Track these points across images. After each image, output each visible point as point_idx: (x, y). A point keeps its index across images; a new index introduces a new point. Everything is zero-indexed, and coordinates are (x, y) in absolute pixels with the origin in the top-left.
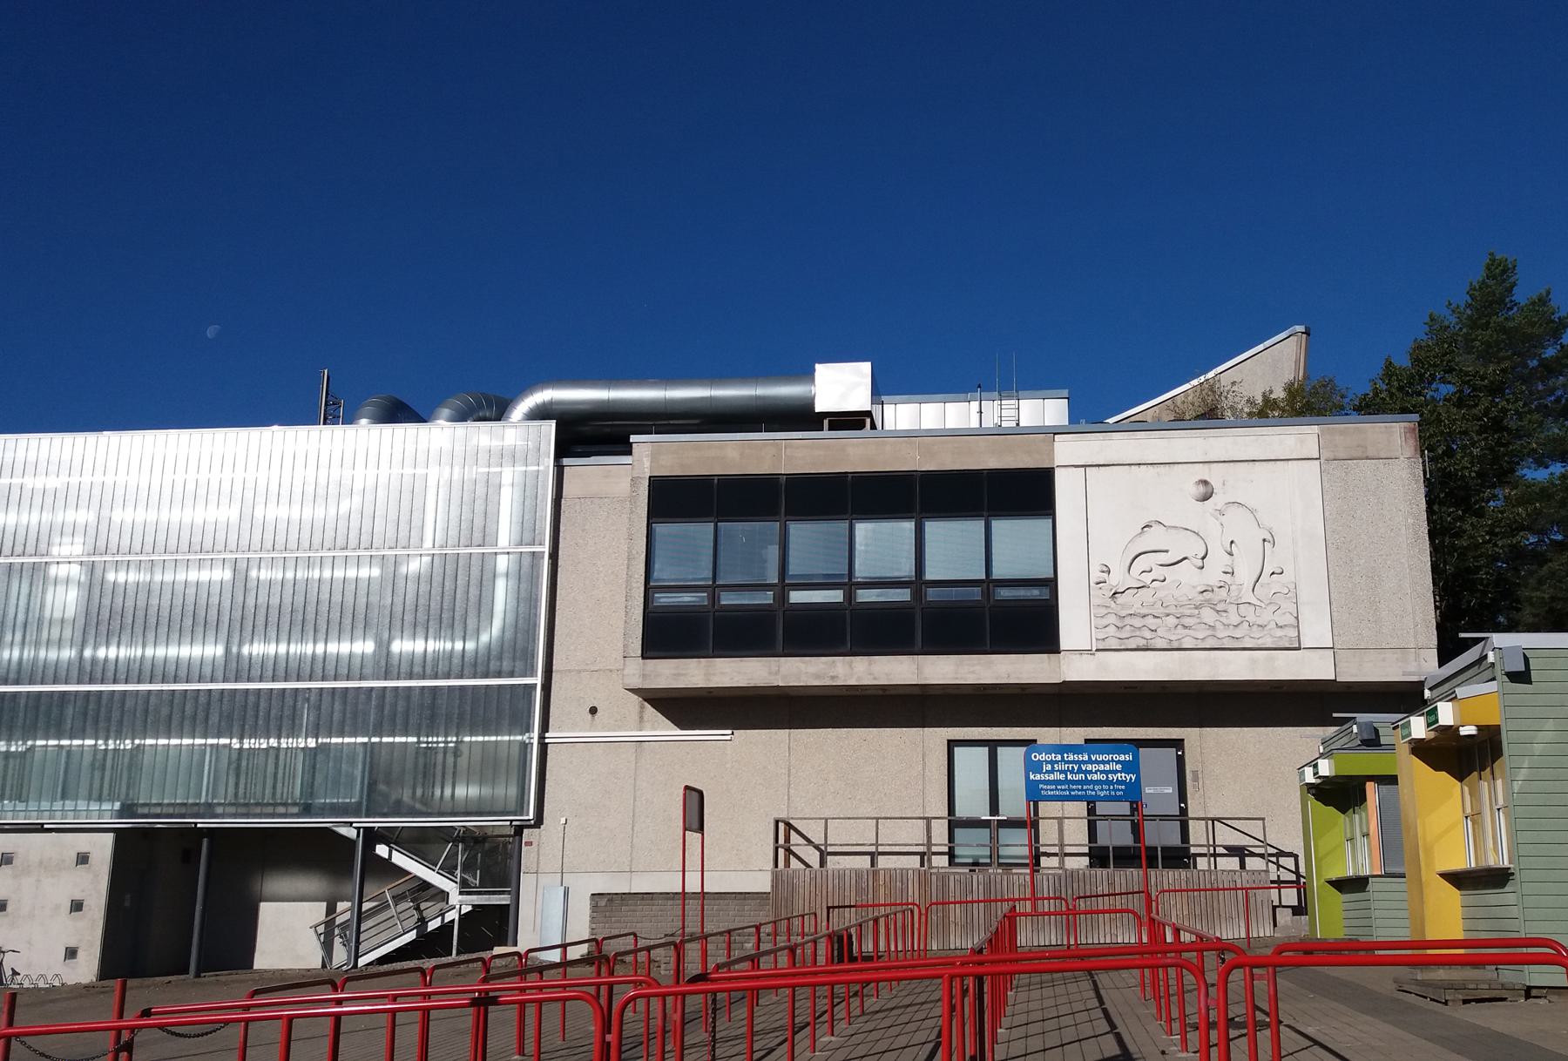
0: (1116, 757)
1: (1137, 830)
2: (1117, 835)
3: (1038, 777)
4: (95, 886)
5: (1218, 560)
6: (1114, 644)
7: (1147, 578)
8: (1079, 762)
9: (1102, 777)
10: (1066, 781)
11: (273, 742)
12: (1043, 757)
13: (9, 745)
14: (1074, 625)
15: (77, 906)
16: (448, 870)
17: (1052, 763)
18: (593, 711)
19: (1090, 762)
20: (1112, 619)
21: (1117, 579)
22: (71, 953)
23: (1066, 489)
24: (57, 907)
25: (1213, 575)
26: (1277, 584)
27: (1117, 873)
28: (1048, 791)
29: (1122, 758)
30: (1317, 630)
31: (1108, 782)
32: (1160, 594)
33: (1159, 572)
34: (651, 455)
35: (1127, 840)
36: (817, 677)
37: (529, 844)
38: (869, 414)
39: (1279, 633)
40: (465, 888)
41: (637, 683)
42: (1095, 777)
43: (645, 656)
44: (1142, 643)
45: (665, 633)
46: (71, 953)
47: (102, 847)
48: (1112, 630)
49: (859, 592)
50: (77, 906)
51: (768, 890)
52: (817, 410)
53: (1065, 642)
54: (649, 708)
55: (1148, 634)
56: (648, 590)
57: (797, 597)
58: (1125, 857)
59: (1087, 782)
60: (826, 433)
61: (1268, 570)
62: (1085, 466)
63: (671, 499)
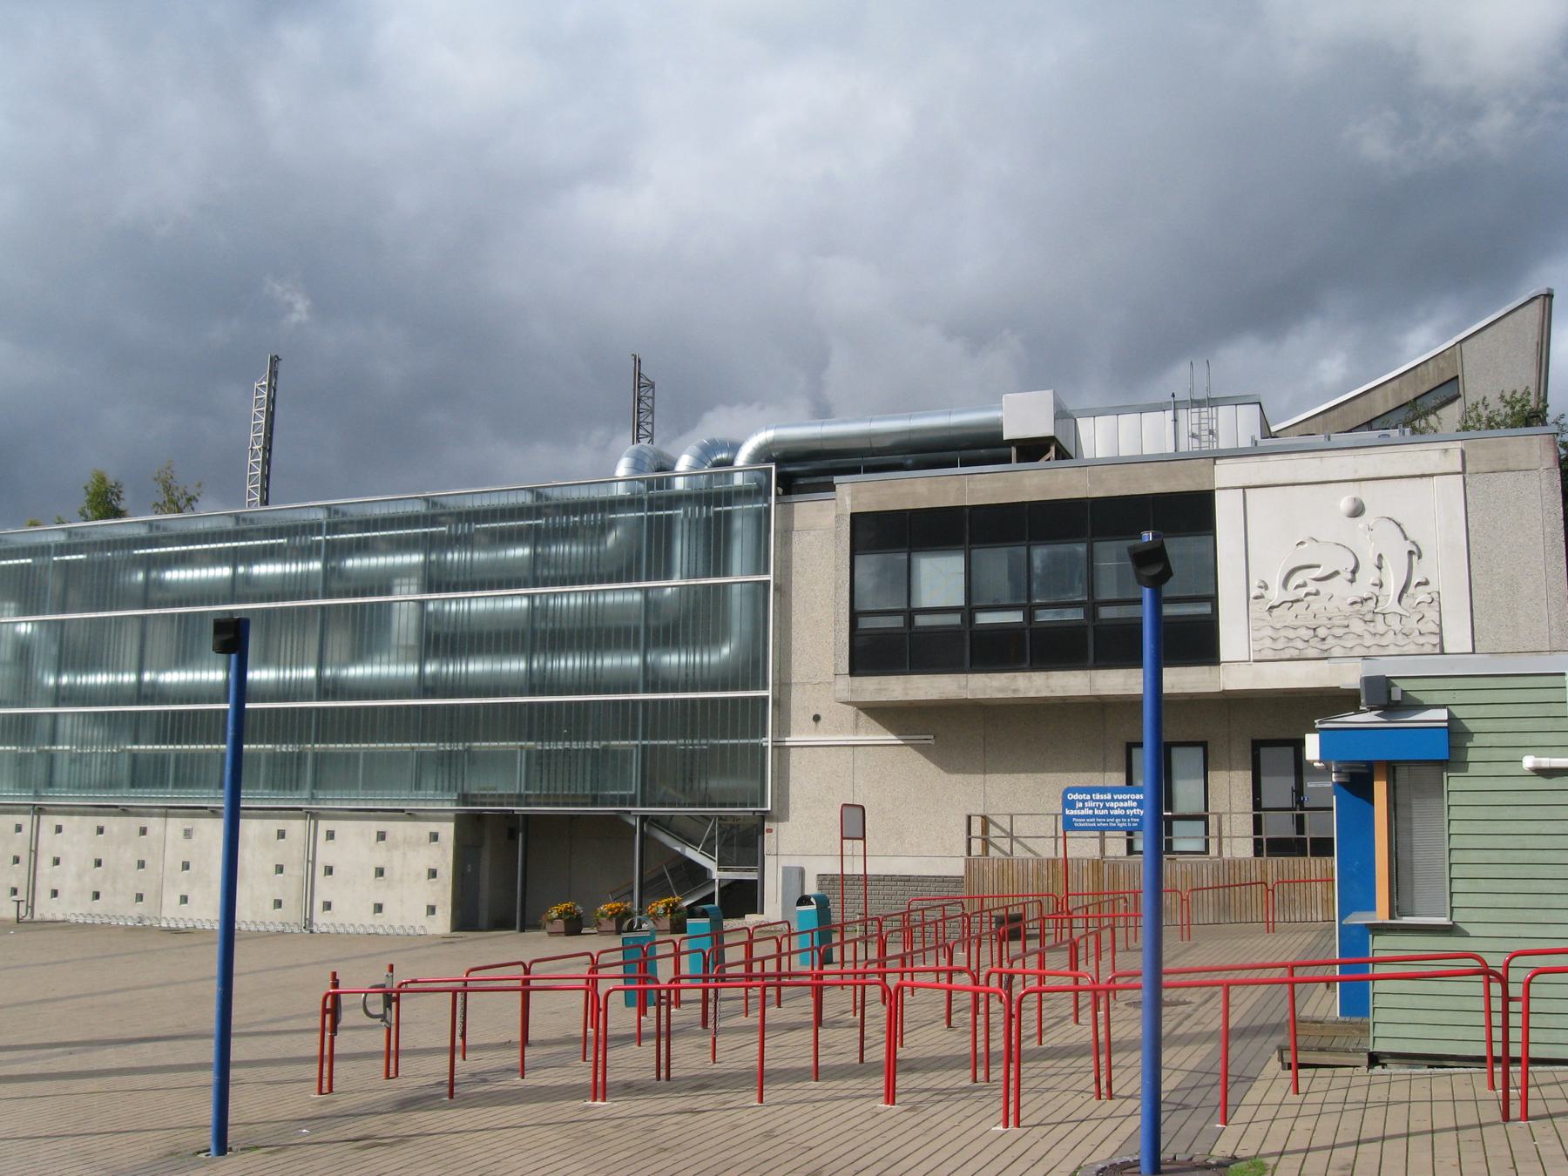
0: (1133, 796)
1: (1300, 824)
2: (1280, 826)
3: (1073, 812)
4: (443, 856)
5: (1368, 575)
6: (1270, 655)
7: (1303, 591)
8: (1104, 801)
9: (1122, 812)
10: (1094, 816)
11: (567, 745)
12: (1076, 796)
13: (235, 568)
14: (1232, 640)
15: (433, 874)
16: (708, 850)
17: (1083, 801)
18: (817, 718)
19: (1113, 800)
20: (1269, 632)
21: (1275, 594)
22: (431, 910)
23: (1226, 510)
24: (419, 875)
25: (1363, 587)
26: (1422, 595)
27: (1270, 860)
28: (1078, 823)
29: (1138, 797)
30: (1458, 638)
31: (1126, 816)
32: (1314, 607)
33: (1311, 588)
34: (855, 494)
35: (1290, 833)
36: (1001, 690)
37: (770, 831)
38: (1052, 439)
39: (1421, 640)
40: (722, 864)
41: (847, 696)
42: (1116, 812)
43: (853, 672)
44: (1295, 653)
45: (869, 653)
46: (431, 910)
47: (447, 830)
48: (1268, 643)
49: (1038, 612)
50: (433, 874)
51: (962, 873)
52: (1006, 437)
53: (1225, 653)
54: (862, 715)
55: (1300, 644)
56: (854, 616)
57: (984, 619)
58: (1280, 847)
59: (1109, 816)
60: (1014, 465)
61: (1414, 581)
62: (1244, 488)
63: (875, 534)
